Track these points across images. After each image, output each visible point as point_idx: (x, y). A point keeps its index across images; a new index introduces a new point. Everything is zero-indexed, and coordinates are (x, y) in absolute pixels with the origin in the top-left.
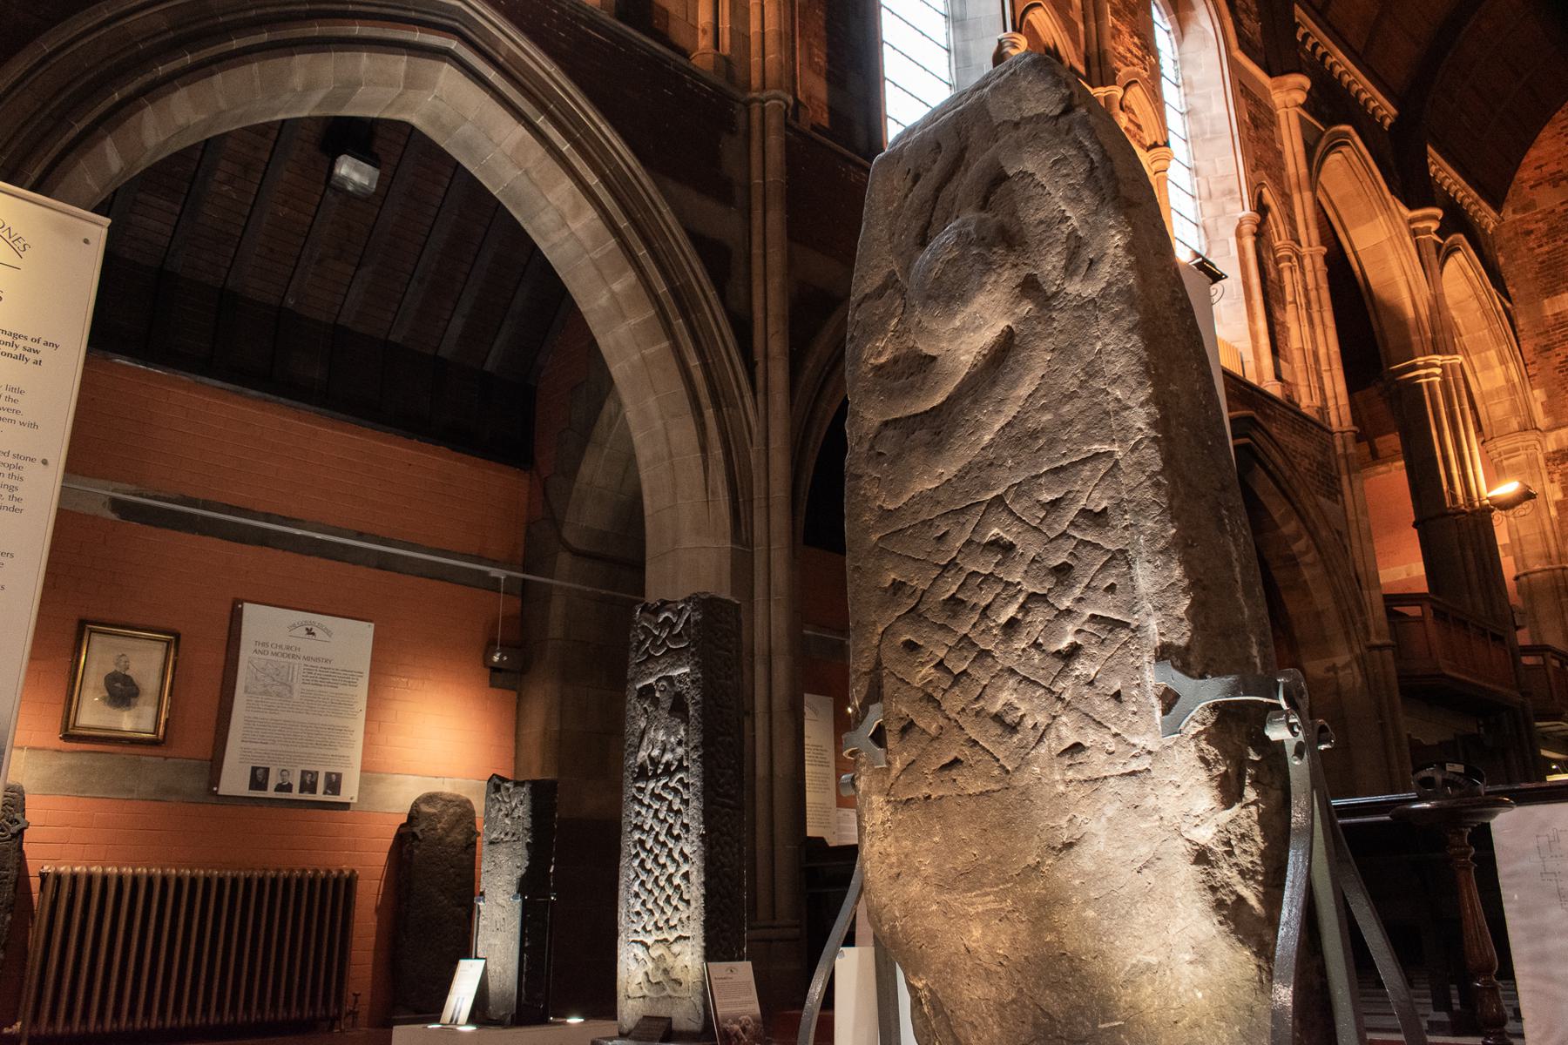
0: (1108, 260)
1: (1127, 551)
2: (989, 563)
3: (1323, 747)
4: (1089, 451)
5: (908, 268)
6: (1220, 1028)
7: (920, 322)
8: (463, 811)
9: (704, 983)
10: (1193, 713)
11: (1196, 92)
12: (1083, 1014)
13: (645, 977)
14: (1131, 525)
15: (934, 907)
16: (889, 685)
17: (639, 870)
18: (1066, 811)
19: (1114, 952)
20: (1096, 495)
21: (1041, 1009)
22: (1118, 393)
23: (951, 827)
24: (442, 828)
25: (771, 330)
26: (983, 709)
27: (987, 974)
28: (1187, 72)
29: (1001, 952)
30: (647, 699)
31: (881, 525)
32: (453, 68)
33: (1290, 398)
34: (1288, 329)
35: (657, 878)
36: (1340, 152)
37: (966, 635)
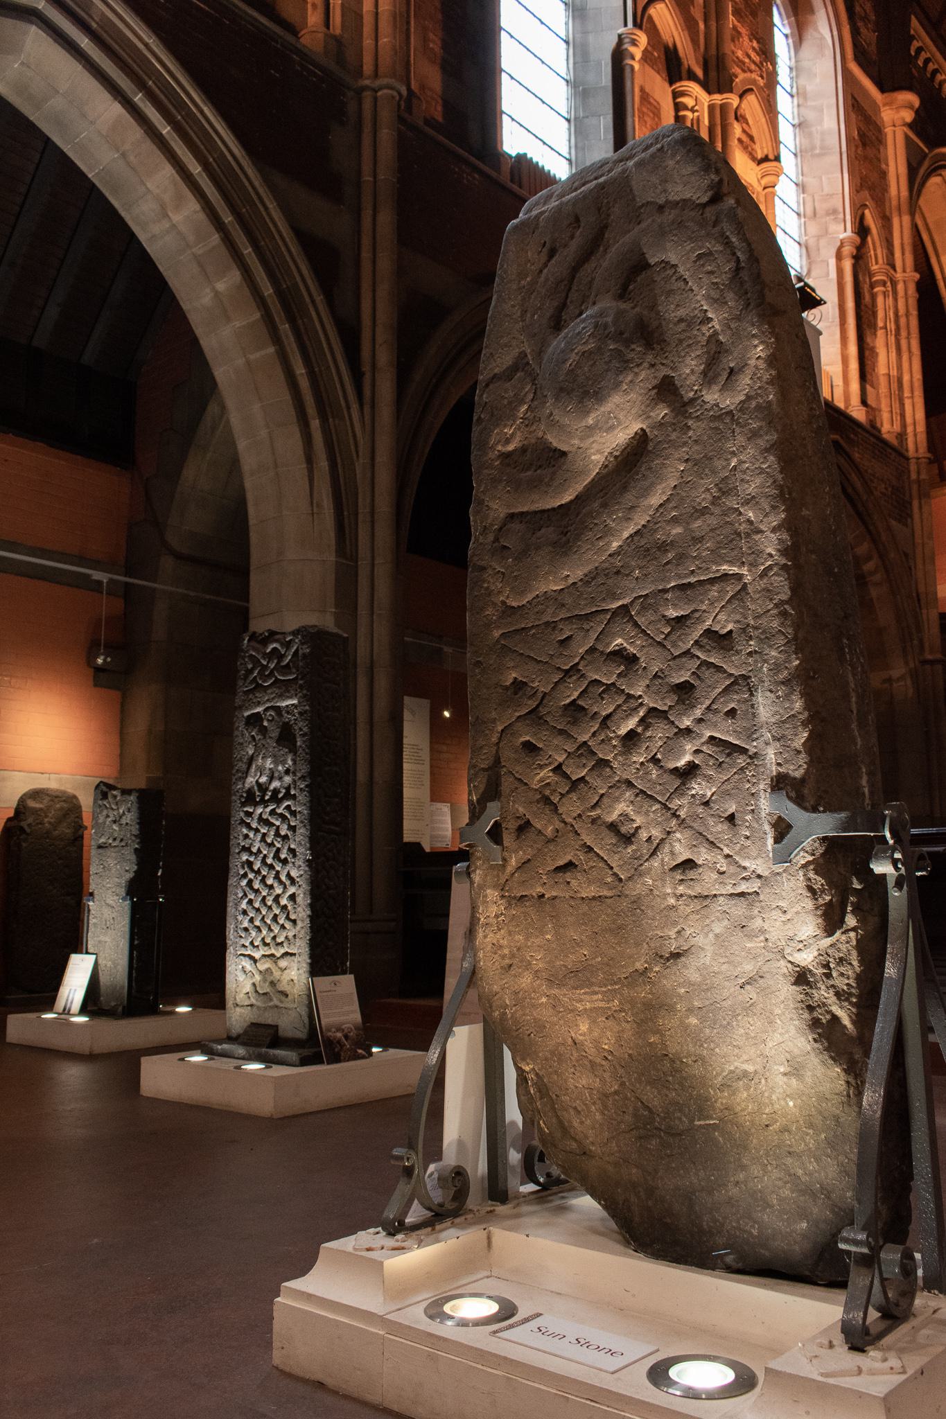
0: (749, 372)
1: (750, 677)
2: (612, 673)
3: (919, 874)
4: (718, 571)
5: (540, 353)
6: (808, 1134)
7: (551, 414)
8: (70, 806)
9: (309, 996)
10: (804, 844)
11: (809, 103)
12: (680, 1111)
13: (253, 988)
14: (756, 652)
15: (544, 1000)
16: (507, 784)
17: (247, 889)
18: (675, 923)
19: (714, 1058)
20: (722, 617)
21: (642, 1102)
22: (751, 514)
23: (564, 926)
24: (50, 823)
25: (379, 340)
26: (599, 817)
27: (592, 1066)
28: (802, 82)
29: (606, 1047)
30: (255, 728)
31: (503, 621)
32: (40, 32)
33: (872, 423)
34: (877, 354)
35: (264, 898)
36: (941, 175)
37: (585, 743)
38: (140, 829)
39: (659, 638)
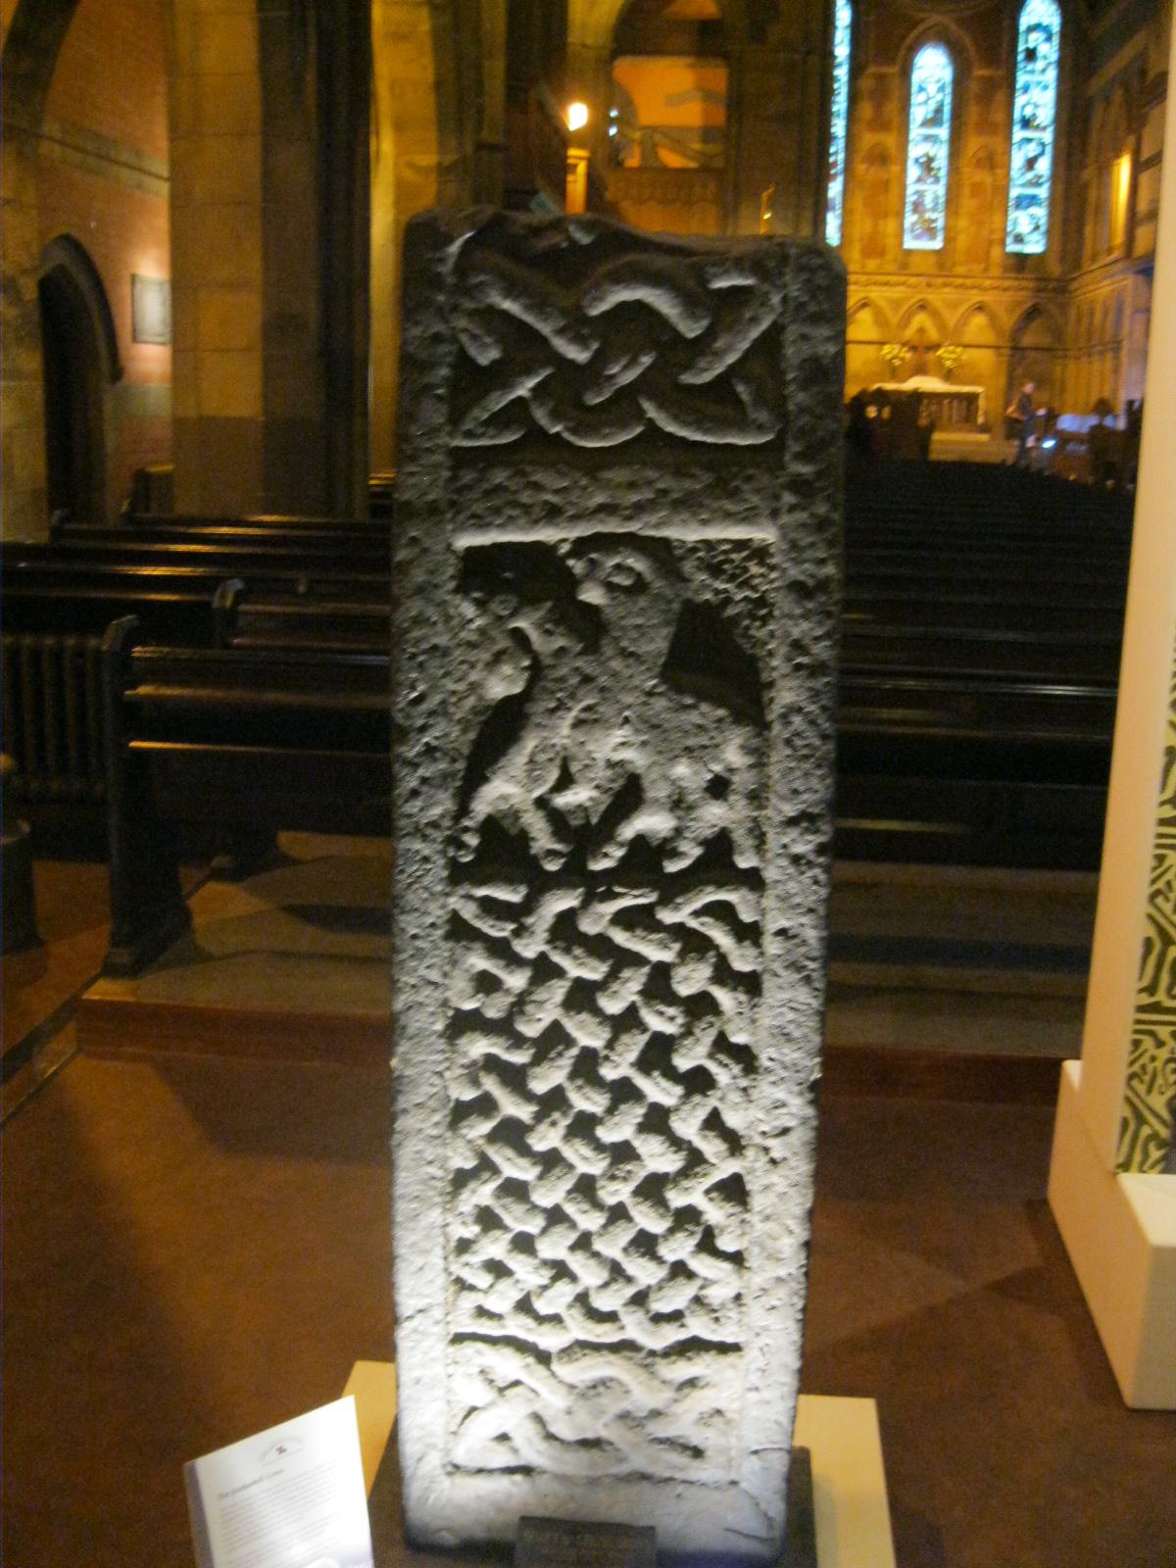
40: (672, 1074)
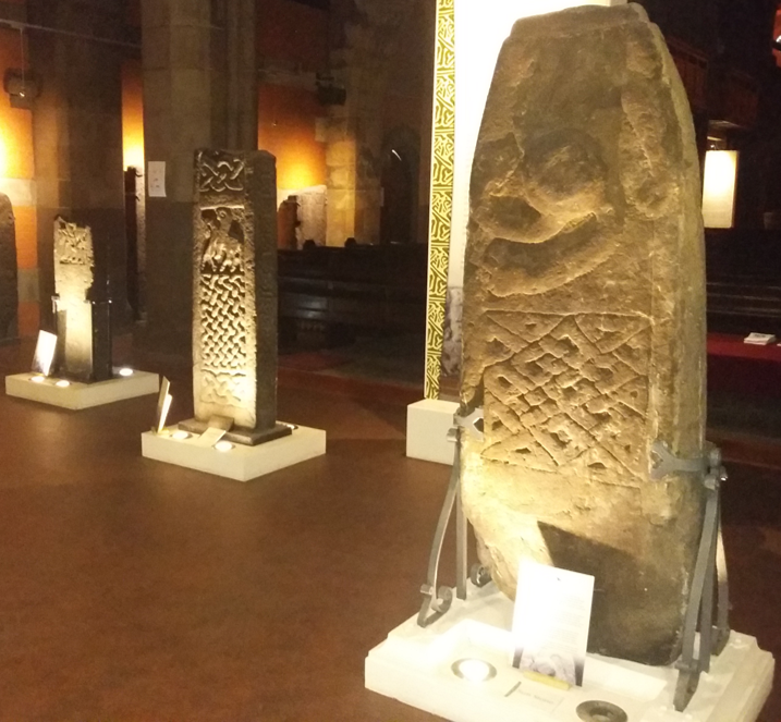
16: (488, 399)
37: (540, 388)
38: (94, 254)
39: (593, 341)
40: (233, 314)
